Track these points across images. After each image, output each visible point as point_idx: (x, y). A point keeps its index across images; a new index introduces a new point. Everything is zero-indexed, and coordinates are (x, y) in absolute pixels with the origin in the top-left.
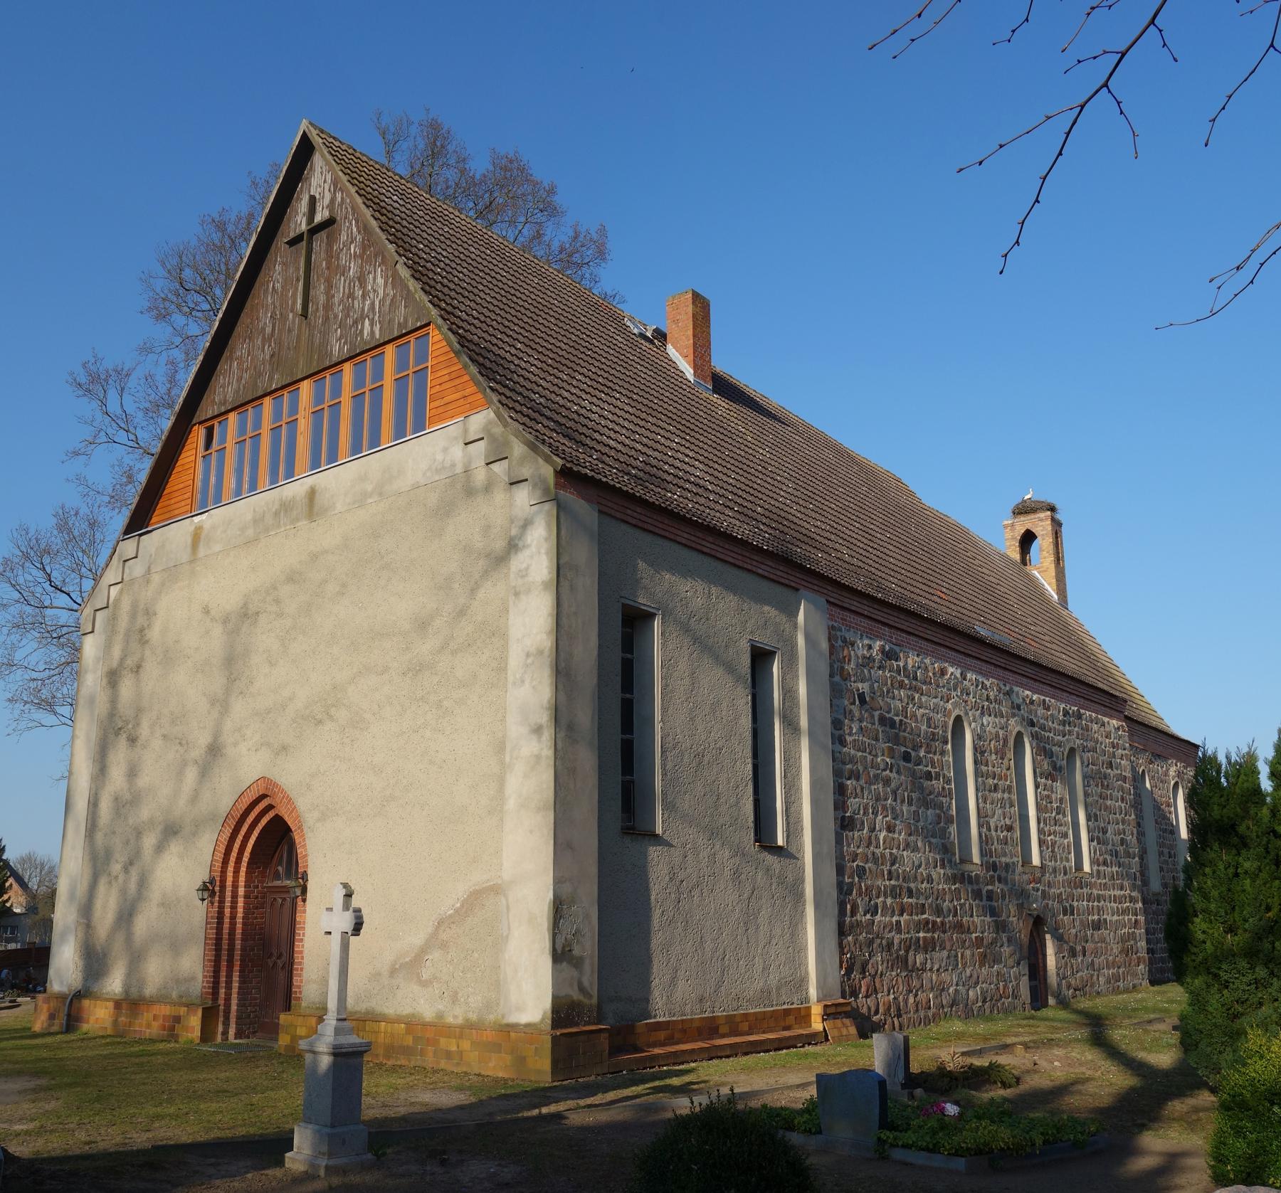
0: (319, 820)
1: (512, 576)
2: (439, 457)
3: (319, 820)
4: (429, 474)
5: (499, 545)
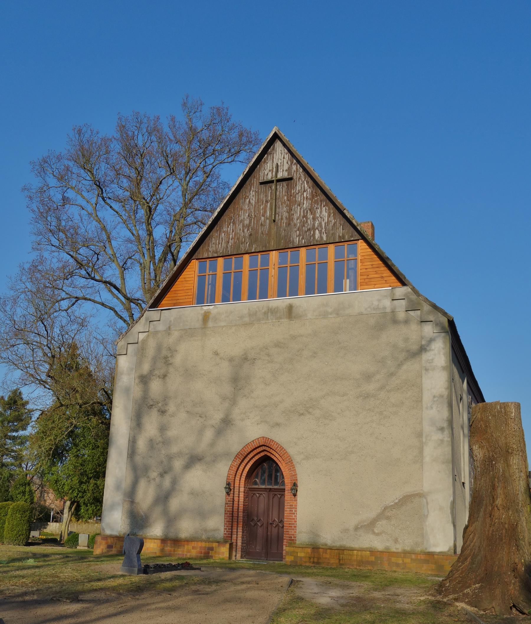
0: (304, 459)
1: (423, 362)
2: (376, 303)
3: (304, 459)
4: (369, 310)
5: (415, 348)
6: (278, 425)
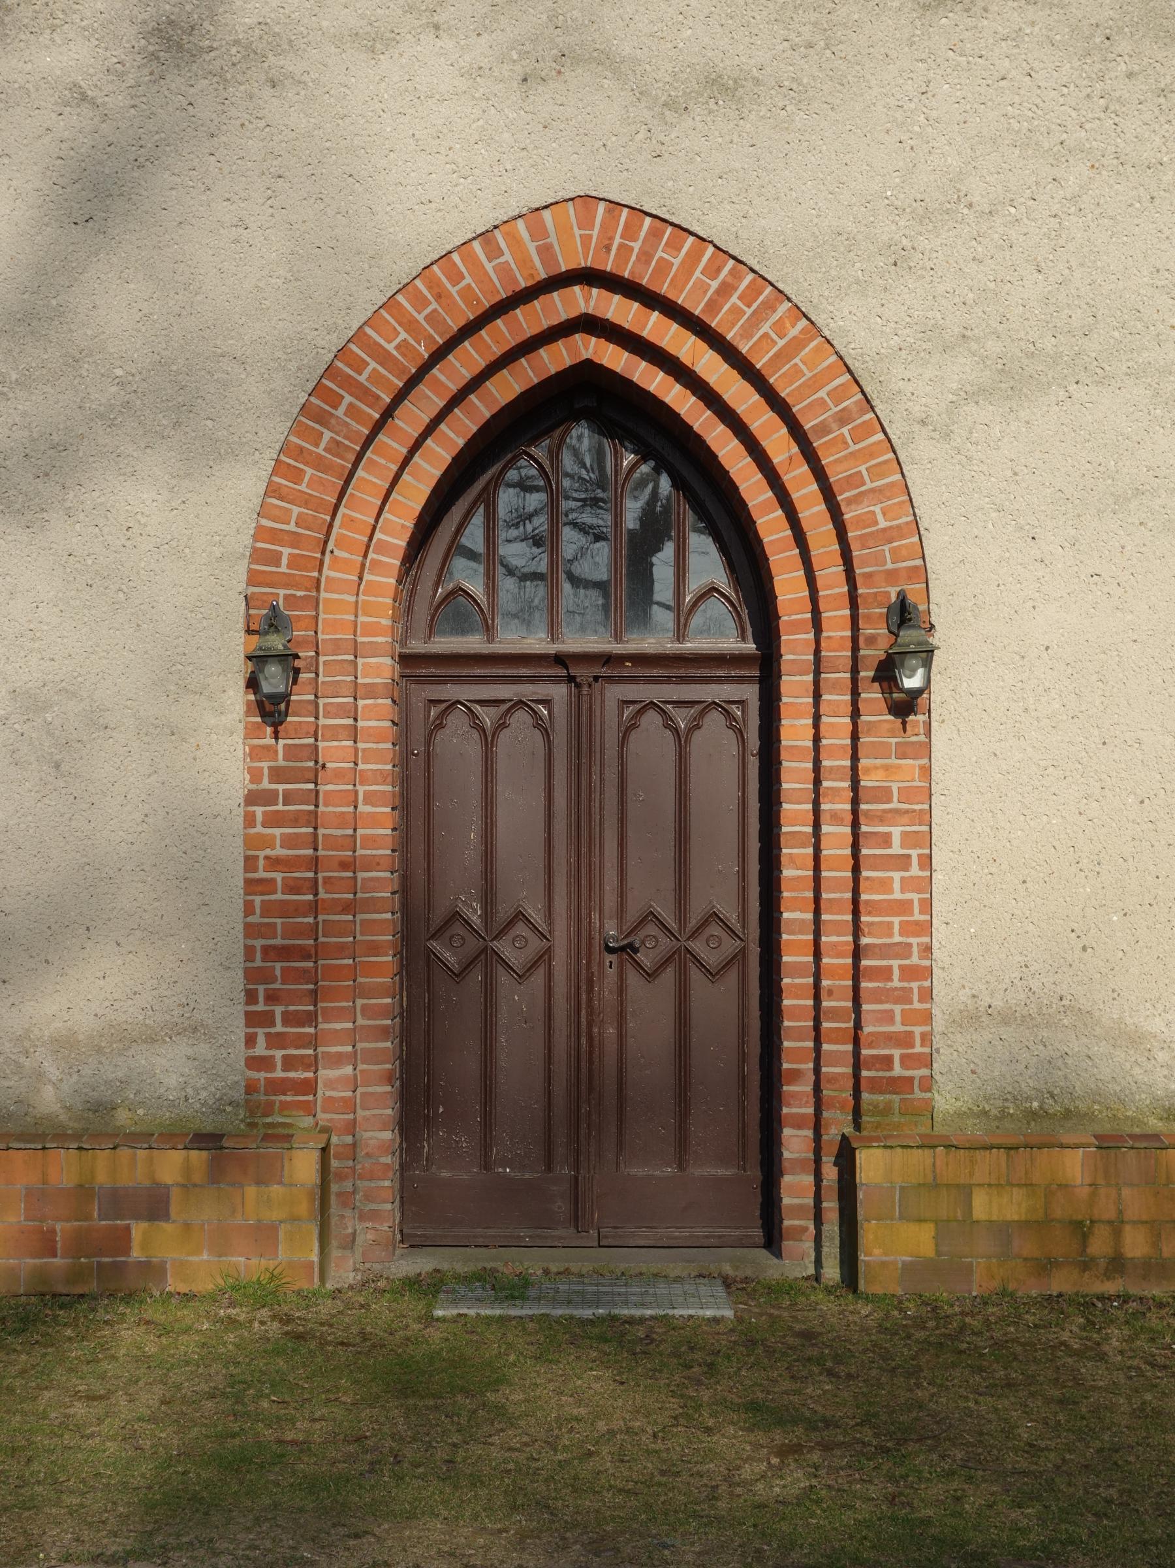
0: (976, 394)
3: (976, 394)
6: (723, 87)
